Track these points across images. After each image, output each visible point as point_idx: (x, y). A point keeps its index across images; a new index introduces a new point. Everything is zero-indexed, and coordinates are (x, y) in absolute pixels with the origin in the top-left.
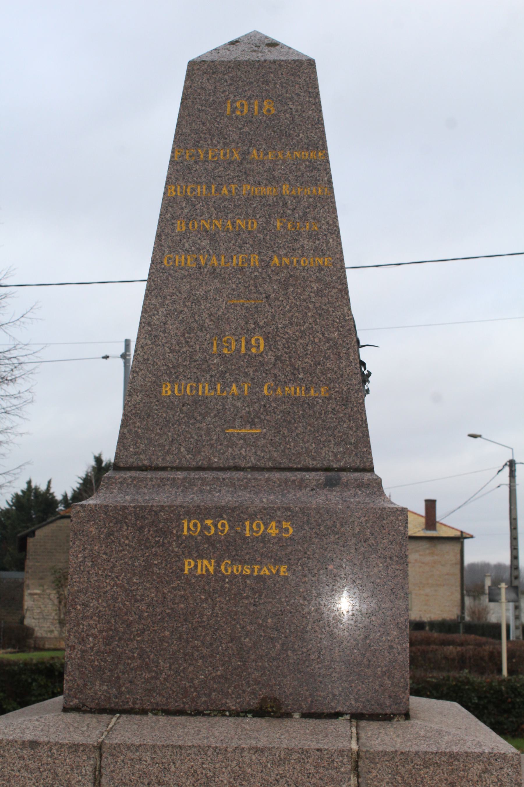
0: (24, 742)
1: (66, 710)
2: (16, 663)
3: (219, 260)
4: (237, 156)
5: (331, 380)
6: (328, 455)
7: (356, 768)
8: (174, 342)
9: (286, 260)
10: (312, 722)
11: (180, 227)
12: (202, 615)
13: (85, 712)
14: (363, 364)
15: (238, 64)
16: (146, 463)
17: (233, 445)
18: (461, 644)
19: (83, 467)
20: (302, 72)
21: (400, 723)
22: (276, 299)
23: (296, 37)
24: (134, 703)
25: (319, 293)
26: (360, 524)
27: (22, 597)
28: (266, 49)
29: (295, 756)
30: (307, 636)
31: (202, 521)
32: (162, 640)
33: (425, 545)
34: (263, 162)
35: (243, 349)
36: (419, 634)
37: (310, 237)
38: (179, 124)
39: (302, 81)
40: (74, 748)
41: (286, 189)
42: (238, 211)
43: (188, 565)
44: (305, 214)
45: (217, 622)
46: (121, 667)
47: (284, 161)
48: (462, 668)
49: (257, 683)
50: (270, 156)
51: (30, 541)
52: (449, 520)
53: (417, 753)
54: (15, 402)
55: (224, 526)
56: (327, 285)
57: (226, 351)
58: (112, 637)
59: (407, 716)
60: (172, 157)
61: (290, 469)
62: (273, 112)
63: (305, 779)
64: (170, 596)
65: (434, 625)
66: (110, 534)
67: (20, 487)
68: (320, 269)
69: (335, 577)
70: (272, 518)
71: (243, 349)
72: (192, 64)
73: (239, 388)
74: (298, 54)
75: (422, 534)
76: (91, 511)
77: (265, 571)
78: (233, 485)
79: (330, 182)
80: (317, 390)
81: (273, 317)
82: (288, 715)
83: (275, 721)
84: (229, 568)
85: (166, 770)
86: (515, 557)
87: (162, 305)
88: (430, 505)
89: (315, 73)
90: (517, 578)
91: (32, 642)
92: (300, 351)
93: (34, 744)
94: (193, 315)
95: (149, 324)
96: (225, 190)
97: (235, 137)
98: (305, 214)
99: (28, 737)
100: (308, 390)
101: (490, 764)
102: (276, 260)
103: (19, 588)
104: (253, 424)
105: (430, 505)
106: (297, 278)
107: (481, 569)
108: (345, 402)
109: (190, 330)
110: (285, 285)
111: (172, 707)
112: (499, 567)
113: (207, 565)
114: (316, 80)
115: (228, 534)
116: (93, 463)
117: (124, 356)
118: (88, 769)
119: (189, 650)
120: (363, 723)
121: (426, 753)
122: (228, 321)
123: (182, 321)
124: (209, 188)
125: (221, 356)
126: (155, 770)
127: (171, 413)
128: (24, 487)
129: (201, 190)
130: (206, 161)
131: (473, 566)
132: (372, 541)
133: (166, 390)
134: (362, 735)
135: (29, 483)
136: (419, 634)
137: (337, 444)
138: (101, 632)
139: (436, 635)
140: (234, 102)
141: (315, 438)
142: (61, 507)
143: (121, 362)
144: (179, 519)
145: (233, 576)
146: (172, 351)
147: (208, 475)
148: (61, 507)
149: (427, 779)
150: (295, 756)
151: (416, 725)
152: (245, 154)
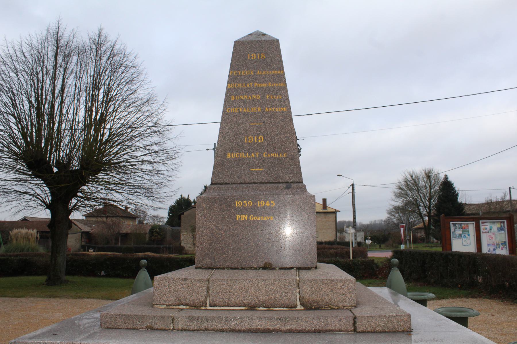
0: (182, 279)
1: (196, 268)
2: (179, 258)
3: (247, 110)
4: (252, 73)
5: (287, 151)
6: (287, 178)
7: (298, 286)
8: (231, 139)
9: (270, 109)
10: (283, 271)
11: (233, 98)
12: (243, 234)
13: (203, 269)
14: (298, 145)
15: (252, 42)
16: (222, 181)
17: (253, 174)
18: (336, 249)
19: (201, 189)
20: (274, 44)
21: (313, 271)
22: (267, 123)
23: (272, 33)
24: (220, 265)
25: (282, 120)
26: (299, 201)
27: (180, 236)
28: (262, 36)
29: (277, 282)
30: (280, 241)
31: (242, 201)
32: (229, 243)
33: (323, 215)
34: (261, 75)
35: (256, 141)
36: (321, 246)
37: (279, 101)
38: (231, 63)
39: (274, 47)
40: (200, 280)
41: (270, 84)
42: (253, 92)
43: (238, 217)
44: (277, 93)
45: (249, 237)
46: (215, 253)
47: (269, 75)
48: (336, 257)
49: (263, 257)
50: (264, 73)
51: (182, 216)
52: (331, 205)
53: (319, 280)
54: (176, 166)
55: (250, 203)
56: (285, 118)
57: (250, 142)
58: (212, 243)
59: (316, 268)
60: (229, 74)
61: (273, 183)
62: (265, 57)
63: (281, 290)
64: (232, 228)
65: (326, 243)
66: (210, 207)
67: (178, 197)
68: (283, 112)
69: (291, 235)
70: (267, 200)
71: (256, 141)
72: (236, 42)
73: (255, 154)
74: (273, 37)
75: (321, 211)
76: (203, 199)
77: (265, 219)
78: (253, 189)
79: (285, 81)
80: (283, 155)
81: (266, 129)
82: (274, 269)
83: (270, 271)
84: (252, 218)
85: (232, 288)
86: (354, 218)
87: (227, 126)
88: (324, 200)
89: (279, 44)
90: (355, 225)
91: (184, 251)
92: (276, 141)
93: (186, 279)
94: (238, 129)
95: (222, 133)
96: (248, 85)
97: (251, 67)
98: (277, 93)
99: (184, 277)
100: (279, 155)
101: (345, 283)
102: (267, 109)
103: (179, 233)
104: (260, 167)
105: (324, 200)
106: (274, 115)
107: (343, 223)
108: (292, 159)
109: (237, 135)
110: (270, 118)
111: (233, 267)
112: (349, 222)
113: (244, 217)
114: (279, 46)
115: (252, 206)
116: (204, 188)
117: (214, 149)
118: (205, 288)
119: (239, 247)
120: (301, 271)
121: (323, 280)
122: (250, 131)
123: (234, 132)
124: (242, 85)
125: (248, 143)
126: (228, 288)
127: (231, 164)
128: (180, 197)
129: (240, 85)
130: (241, 75)
131: (340, 222)
132: (303, 207)
133: (229, 156)
134: (300, 274)
135: (181, 196)
136: (321, 246)
137: (290, 174)
138: (208, 241)
139: (327, 246)
140: (251, 55)
141: (282, 172)
142: (193, 204)
143: (213, 151)
144: (234, 201)
145: (254, 221)
146: (231, 142)
147: (245, 186)
148: (193, 204)
149: (323, 288)
150: (277, 282)
151: (319, 271)
152: (255, 72)
